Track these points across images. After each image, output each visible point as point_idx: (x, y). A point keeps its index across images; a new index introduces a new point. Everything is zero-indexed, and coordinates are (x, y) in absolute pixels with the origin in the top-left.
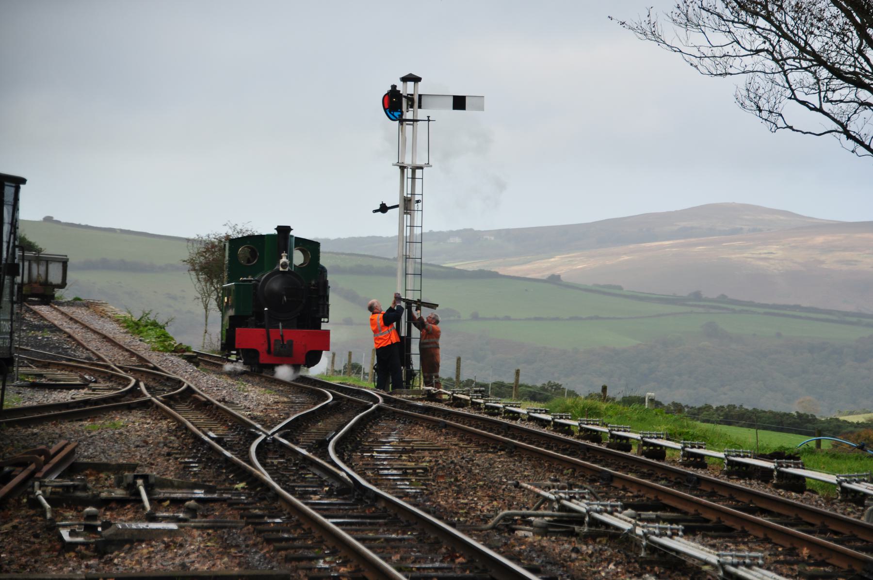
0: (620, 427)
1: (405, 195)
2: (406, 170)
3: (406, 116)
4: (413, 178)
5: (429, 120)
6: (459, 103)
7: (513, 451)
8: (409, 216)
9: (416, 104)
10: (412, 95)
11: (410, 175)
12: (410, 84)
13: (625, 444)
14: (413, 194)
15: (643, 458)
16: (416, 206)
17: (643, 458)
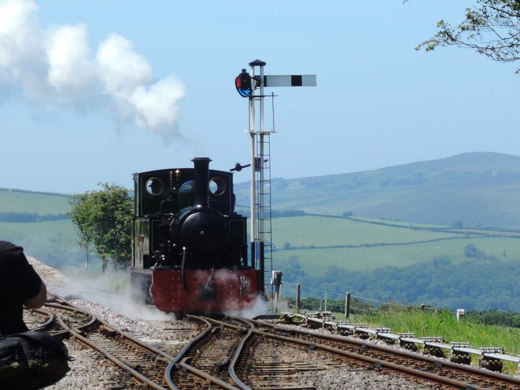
0: (461, 344)
1: (256, 156)
2: (255, 136)
3: (254, 94)
4: (262, 142)
5: (273, 96)
6: (297, 81)
7: (372, 367)
8: (259, 172)
9: (262, 84)
10: (259, 76)
11: (259, 141)
12: (257, 68)
13: (465, 358)
14: (262, 155)
15: (484, 370)
16: (265, 165)
17: (484, 370)
